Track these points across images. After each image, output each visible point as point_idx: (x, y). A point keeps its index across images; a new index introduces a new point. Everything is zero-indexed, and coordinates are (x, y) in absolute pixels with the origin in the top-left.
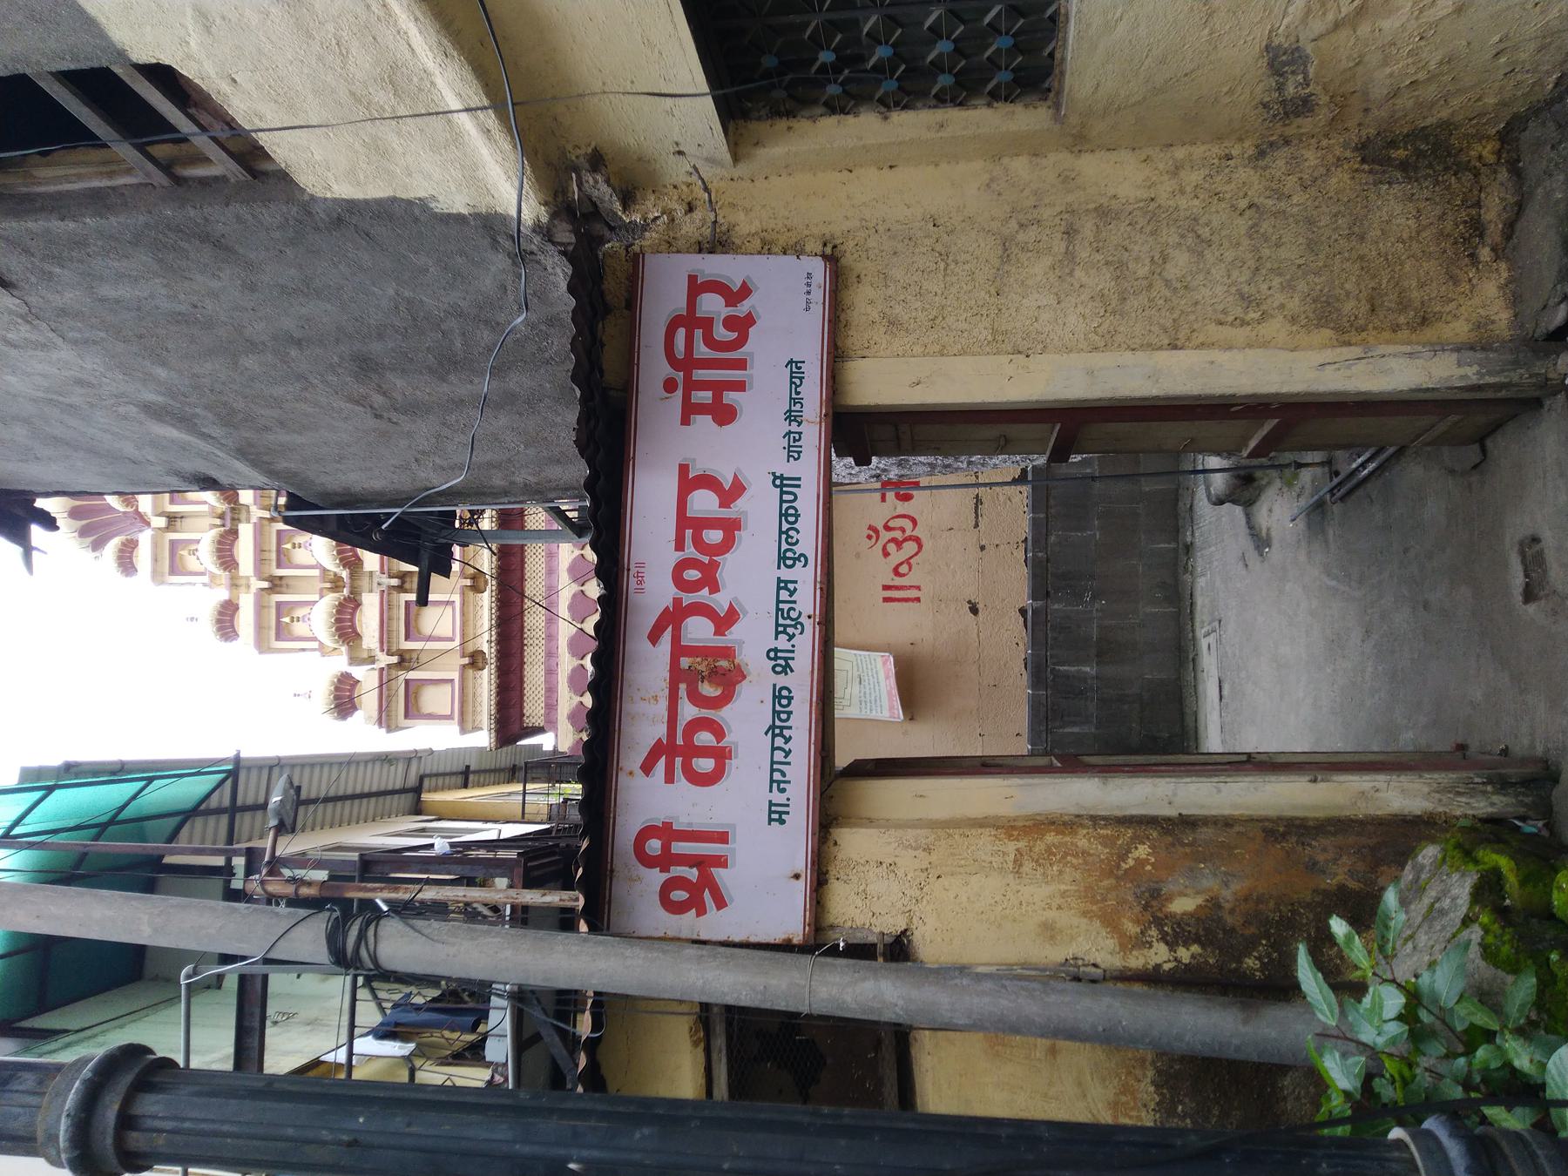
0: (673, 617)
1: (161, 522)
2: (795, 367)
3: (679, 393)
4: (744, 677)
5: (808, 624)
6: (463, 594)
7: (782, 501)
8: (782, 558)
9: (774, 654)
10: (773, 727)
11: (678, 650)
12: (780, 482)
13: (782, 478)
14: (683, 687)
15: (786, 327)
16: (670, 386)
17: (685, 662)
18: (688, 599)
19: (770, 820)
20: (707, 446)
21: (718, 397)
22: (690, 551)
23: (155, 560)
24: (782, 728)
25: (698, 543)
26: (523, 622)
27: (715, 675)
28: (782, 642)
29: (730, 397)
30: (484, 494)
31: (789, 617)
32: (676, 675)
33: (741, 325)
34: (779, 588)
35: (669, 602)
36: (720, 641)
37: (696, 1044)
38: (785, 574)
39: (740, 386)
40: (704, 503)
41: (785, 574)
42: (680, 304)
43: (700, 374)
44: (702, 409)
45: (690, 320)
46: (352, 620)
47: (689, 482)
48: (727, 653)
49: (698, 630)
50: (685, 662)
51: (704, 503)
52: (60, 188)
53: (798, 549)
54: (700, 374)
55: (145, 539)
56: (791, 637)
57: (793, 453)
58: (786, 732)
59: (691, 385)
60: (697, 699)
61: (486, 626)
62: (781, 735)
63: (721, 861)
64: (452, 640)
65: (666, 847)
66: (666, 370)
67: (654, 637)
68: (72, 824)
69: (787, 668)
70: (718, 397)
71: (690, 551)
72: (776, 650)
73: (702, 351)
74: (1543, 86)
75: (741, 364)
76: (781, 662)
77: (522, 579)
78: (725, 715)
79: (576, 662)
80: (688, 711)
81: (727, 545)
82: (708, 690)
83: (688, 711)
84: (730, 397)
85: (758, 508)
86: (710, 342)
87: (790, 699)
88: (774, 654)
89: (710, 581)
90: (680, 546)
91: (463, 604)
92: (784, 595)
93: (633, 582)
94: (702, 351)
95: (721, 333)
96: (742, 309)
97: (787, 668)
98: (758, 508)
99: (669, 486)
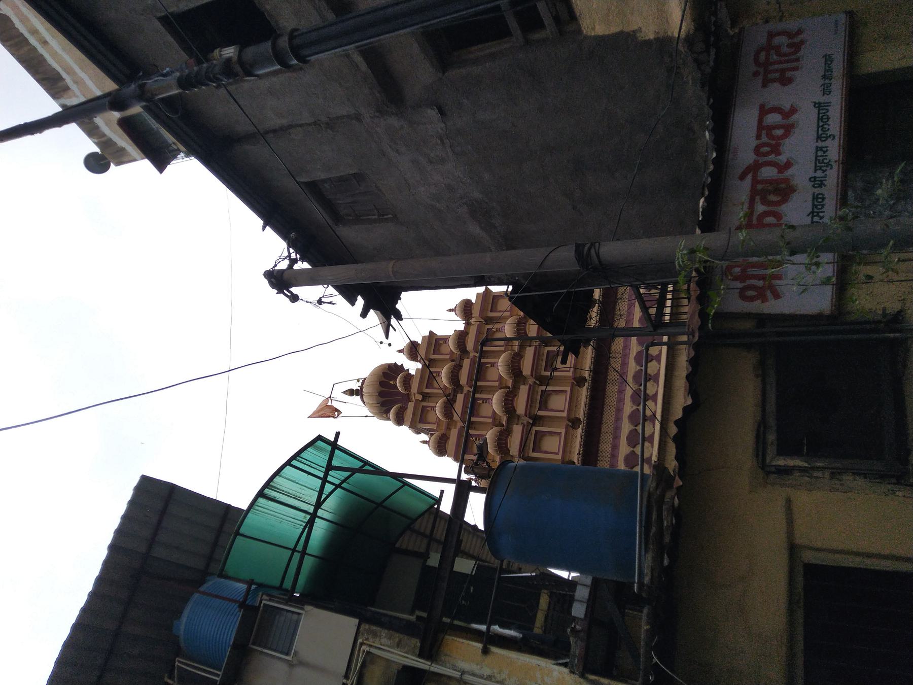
0: (755, 168)
1: (420, 397)
2: (828, 59)
4: (795, 191)
5: (835, 166)
6: (567, 428)
7: (819, 114)
8: (819, 138)
9: (813, 179)
10: (812, 212)
11: (755, 181)
12: (818, 105)
13: (819, 103)
14: (758, 198)
15: (823, 41)
16: (756, 74)
17: (759, 187)
18: (762, 160)
20: (778, 95)
22: (765, 139)
23: (414, 414)
24: (818, 213)
25: (770, 136)
26: (598, 447)
27: (776, 191)
28: (819, 174)
29: (789, 74)
31: (823, 162)
32: (754, 193)
33: (797, 47)
34: (817, 151)
35: (751, 161)
36: (781, 176)
37: (757, 376)
38: (820, 144)
40: (773, 118)
41: (820, 144)
42: (763, 41)
44: (774, 80)
45: (769, 47)
46: (506, 440)
47: (764, 111)
48: (787, 180)
49: (768, 173)
50: (759, 187)
51: (773, 118)
53: (829, 133)
55: (411, 406)
56: (824, 171)
57: (826, 90)
58: (821, 214)
60: (764, 202)
61: (577, 451)
62: (818, 215)
63: (779, 277)
64: (557, 454)
65: (744, 271)
66: (753, 68)
67: (742, 177)
68: (366, 495)
69: (821, 185)
71: (765, 139)
72: (815, 177)
76: (818, 182)
77: (601, 423)
78: (784, 208)
79: (632, 427)
80: (760, 208)
81: (786, 135)
82: (773, 198)
83: (760, 208)
84: (789, 74)
85: (806, 119)
86: (779, 54)
87: (823, 199)
88: (813, 179)
89: (776, 150)
90: (758, 137)
91: (566, 433)
92: (820, 153)
93: (731, 156)
95: (785, 50)
96: (797, 40)
97: (821, 185)
98: (806, 119)
99: (755, 113)
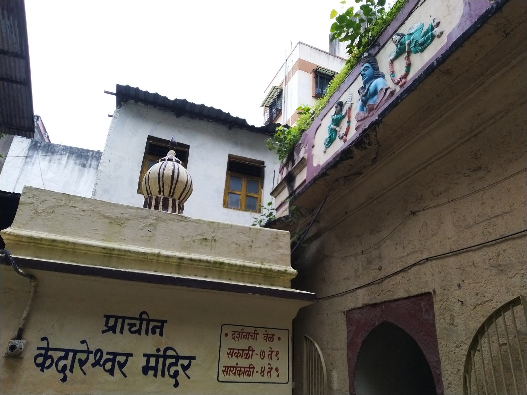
3: (156, 353)
19: (108, 317)
21: (152, 368)
22: (105, 357)
29: (151, 373)
30: (140, 261)
39: (155, 375)
43: (161, 360)
44: (148, 362)
52: (305, 385)
54: (161, 360)
59: (157, 357)
70: (152, 368)
71: (105, 357)
73: (169, 361)
74: (296, 153)
75: (163, 375)
84: (151, 373)
90: (108, 353)
94: (169, 361)
